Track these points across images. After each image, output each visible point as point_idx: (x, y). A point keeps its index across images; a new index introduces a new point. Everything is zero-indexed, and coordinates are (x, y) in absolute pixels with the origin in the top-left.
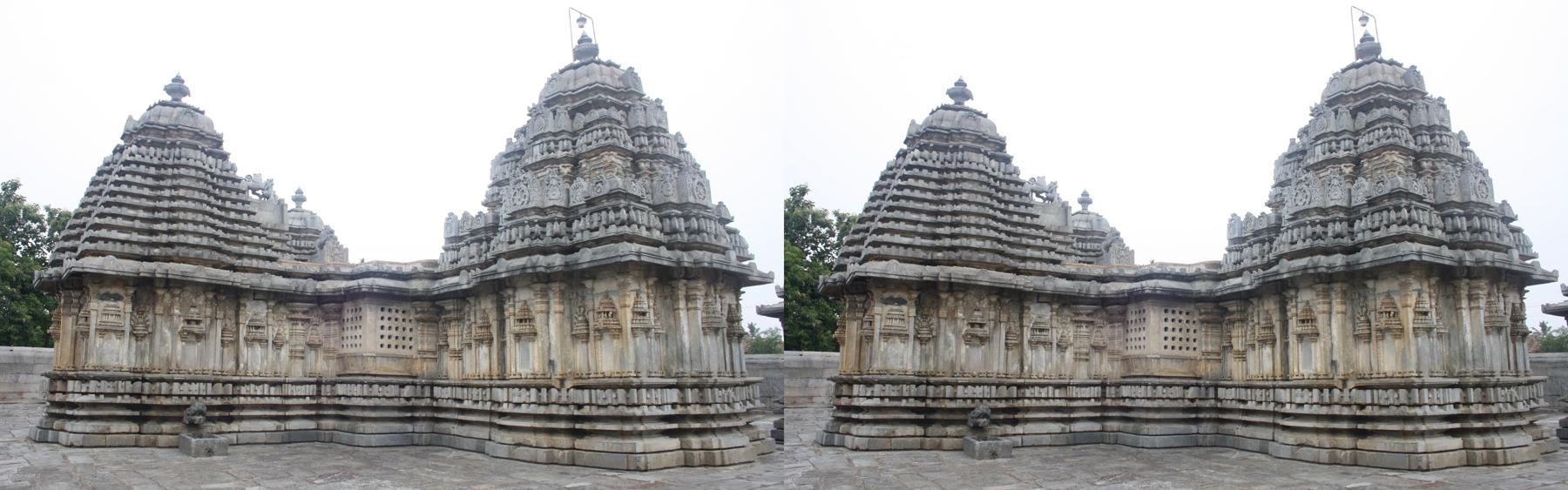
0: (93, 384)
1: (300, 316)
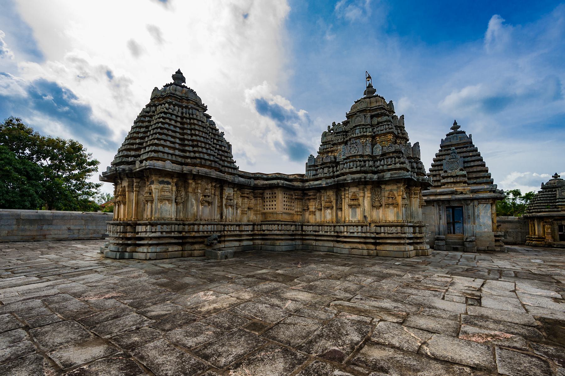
0: (159, 227)
1: (246, 195)
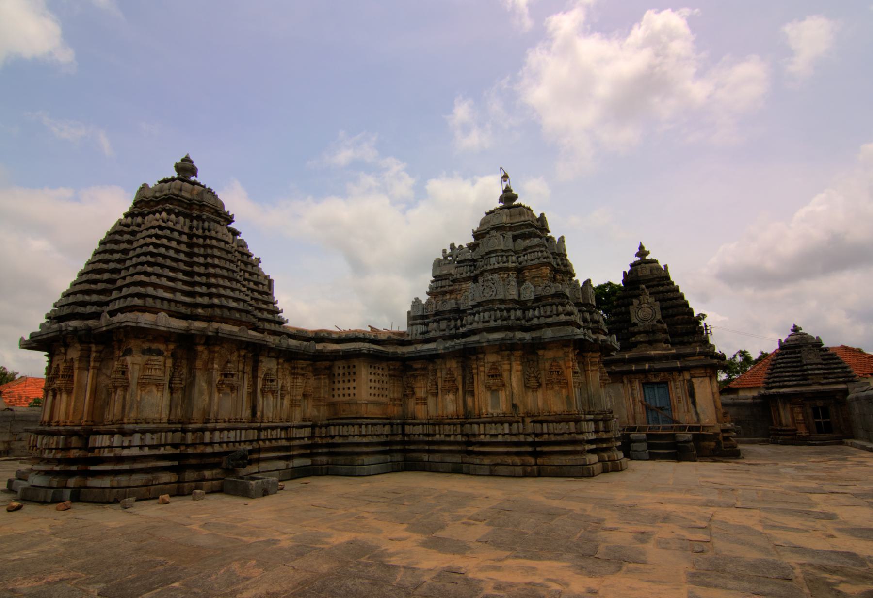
1: (300, 371)
